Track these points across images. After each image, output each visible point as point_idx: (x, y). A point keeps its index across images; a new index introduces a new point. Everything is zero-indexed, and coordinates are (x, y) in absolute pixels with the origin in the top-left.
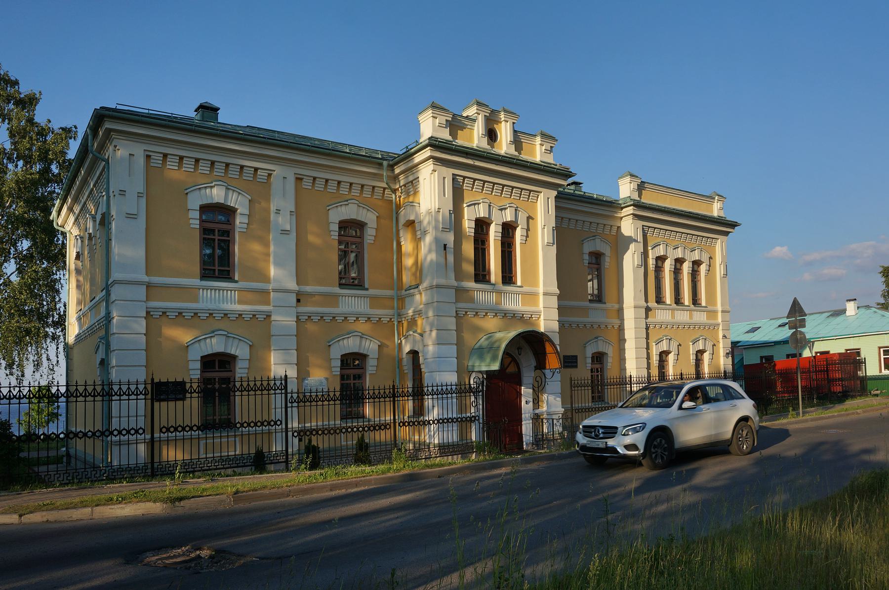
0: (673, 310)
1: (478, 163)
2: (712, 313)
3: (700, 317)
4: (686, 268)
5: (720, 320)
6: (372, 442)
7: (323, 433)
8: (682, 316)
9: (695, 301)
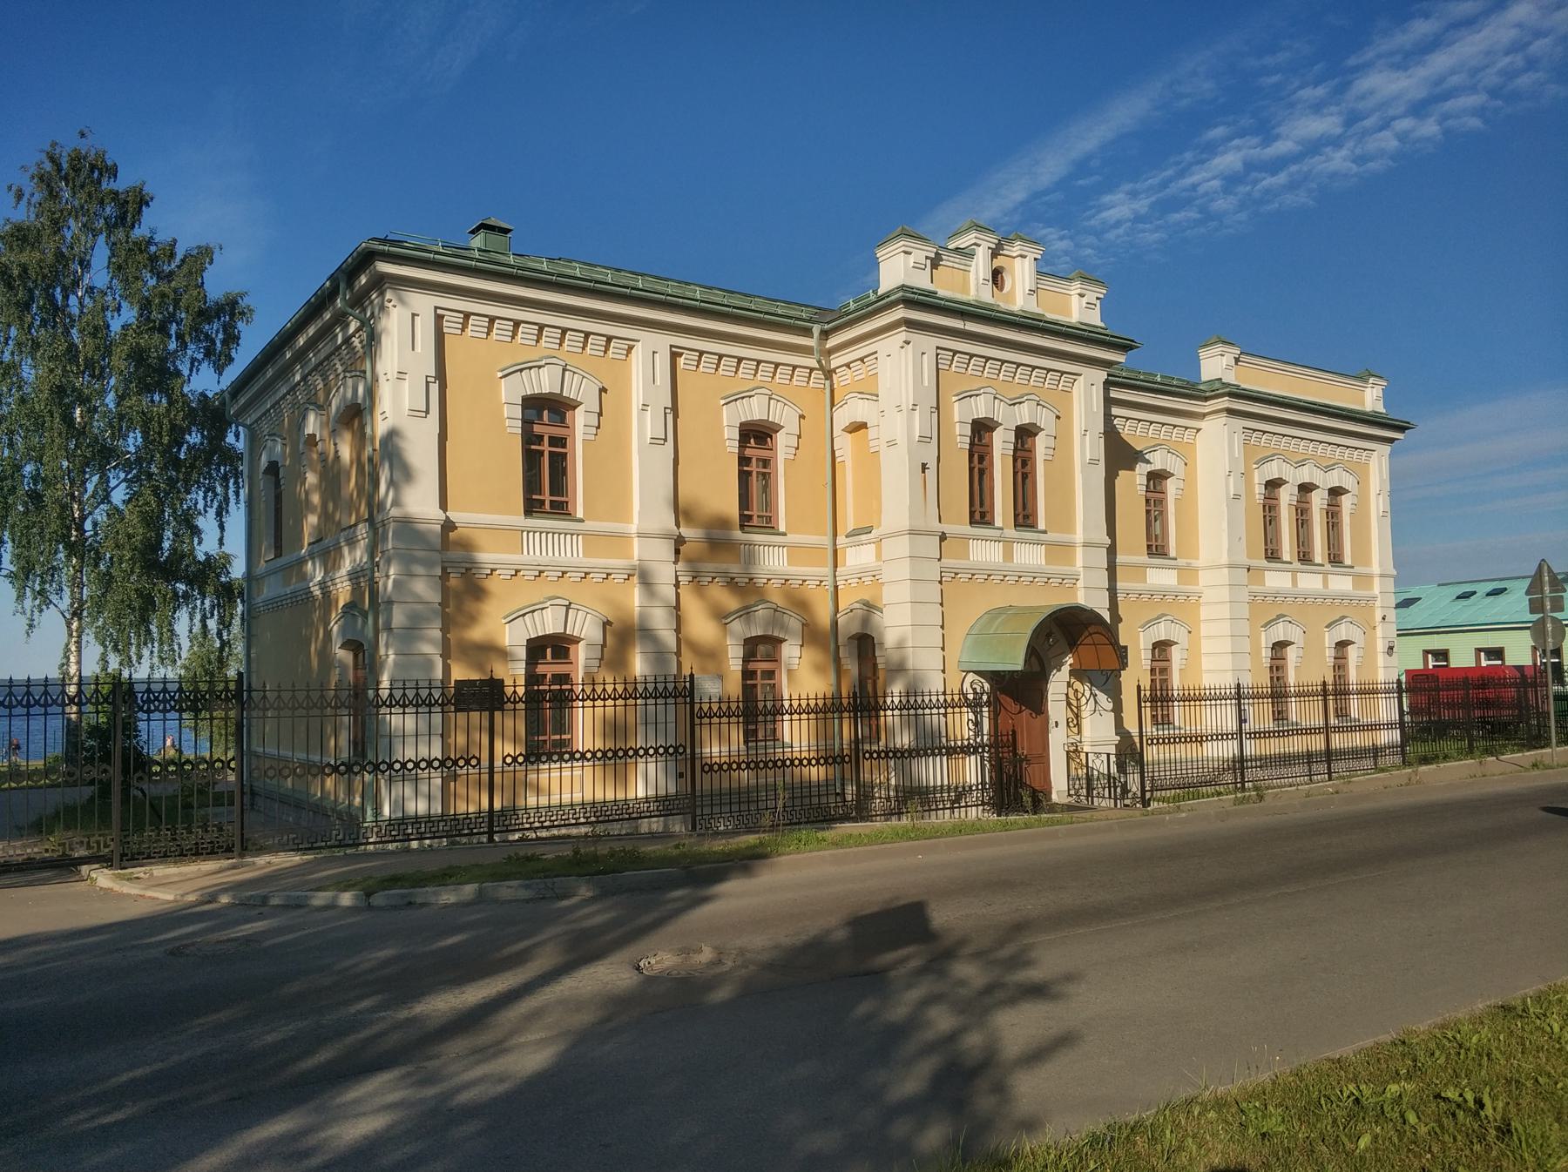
0: (1326, 574)
1: (972, 327)
2: (1363, 580)
3: (1341, 584)
4: (1318, 500)
5: (1376, 590)
6: (735, 785)
7: (887, 756)
8: (1310, 582)
9: (1335, 559)
